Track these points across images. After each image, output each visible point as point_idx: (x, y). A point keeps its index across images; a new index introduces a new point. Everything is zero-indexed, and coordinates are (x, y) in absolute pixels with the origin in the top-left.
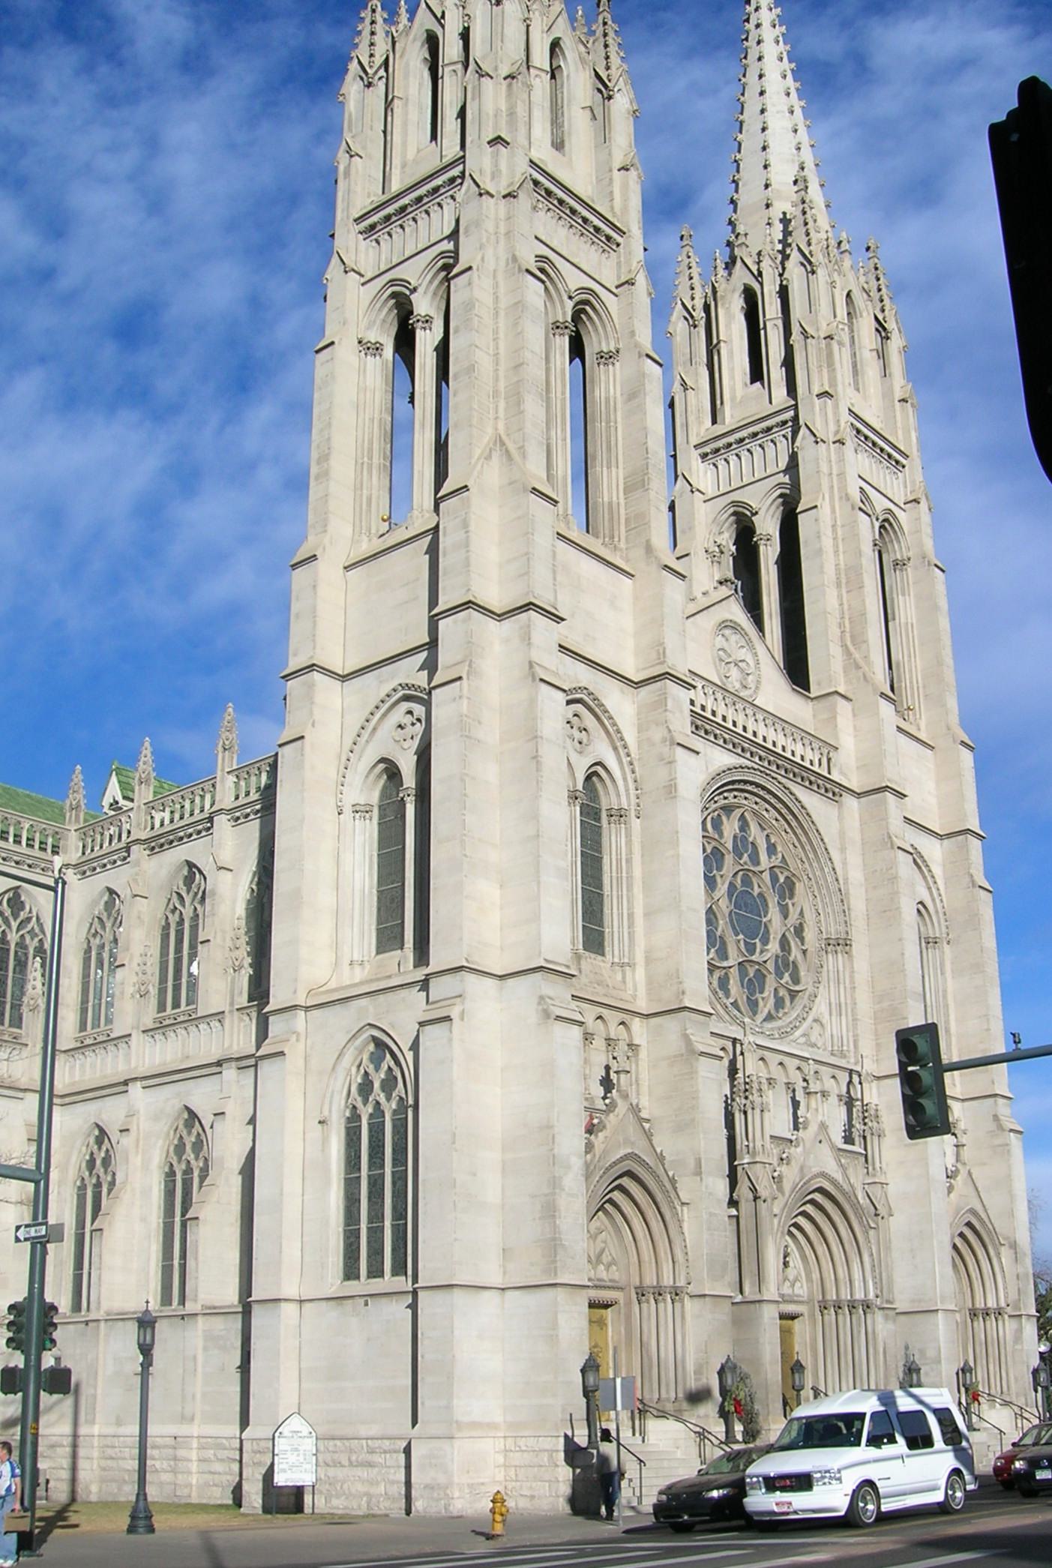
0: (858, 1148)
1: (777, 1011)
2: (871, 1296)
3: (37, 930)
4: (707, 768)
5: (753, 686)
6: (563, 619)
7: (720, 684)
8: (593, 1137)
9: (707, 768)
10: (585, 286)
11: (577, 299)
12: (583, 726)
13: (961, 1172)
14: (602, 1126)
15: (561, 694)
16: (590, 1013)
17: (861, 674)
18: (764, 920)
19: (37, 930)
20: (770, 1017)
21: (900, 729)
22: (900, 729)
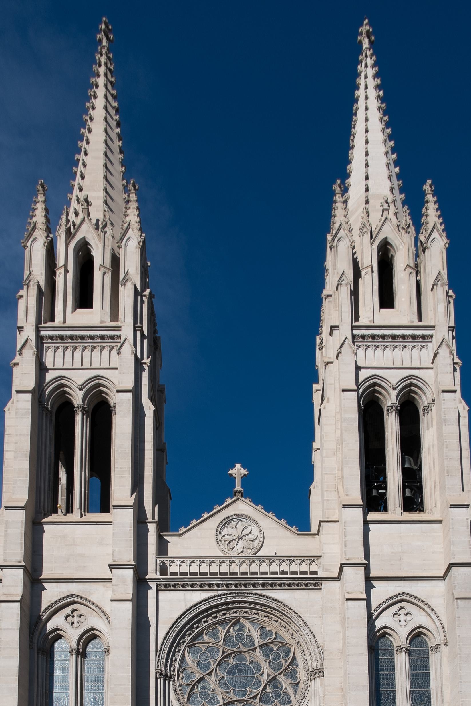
18: (248, 663)
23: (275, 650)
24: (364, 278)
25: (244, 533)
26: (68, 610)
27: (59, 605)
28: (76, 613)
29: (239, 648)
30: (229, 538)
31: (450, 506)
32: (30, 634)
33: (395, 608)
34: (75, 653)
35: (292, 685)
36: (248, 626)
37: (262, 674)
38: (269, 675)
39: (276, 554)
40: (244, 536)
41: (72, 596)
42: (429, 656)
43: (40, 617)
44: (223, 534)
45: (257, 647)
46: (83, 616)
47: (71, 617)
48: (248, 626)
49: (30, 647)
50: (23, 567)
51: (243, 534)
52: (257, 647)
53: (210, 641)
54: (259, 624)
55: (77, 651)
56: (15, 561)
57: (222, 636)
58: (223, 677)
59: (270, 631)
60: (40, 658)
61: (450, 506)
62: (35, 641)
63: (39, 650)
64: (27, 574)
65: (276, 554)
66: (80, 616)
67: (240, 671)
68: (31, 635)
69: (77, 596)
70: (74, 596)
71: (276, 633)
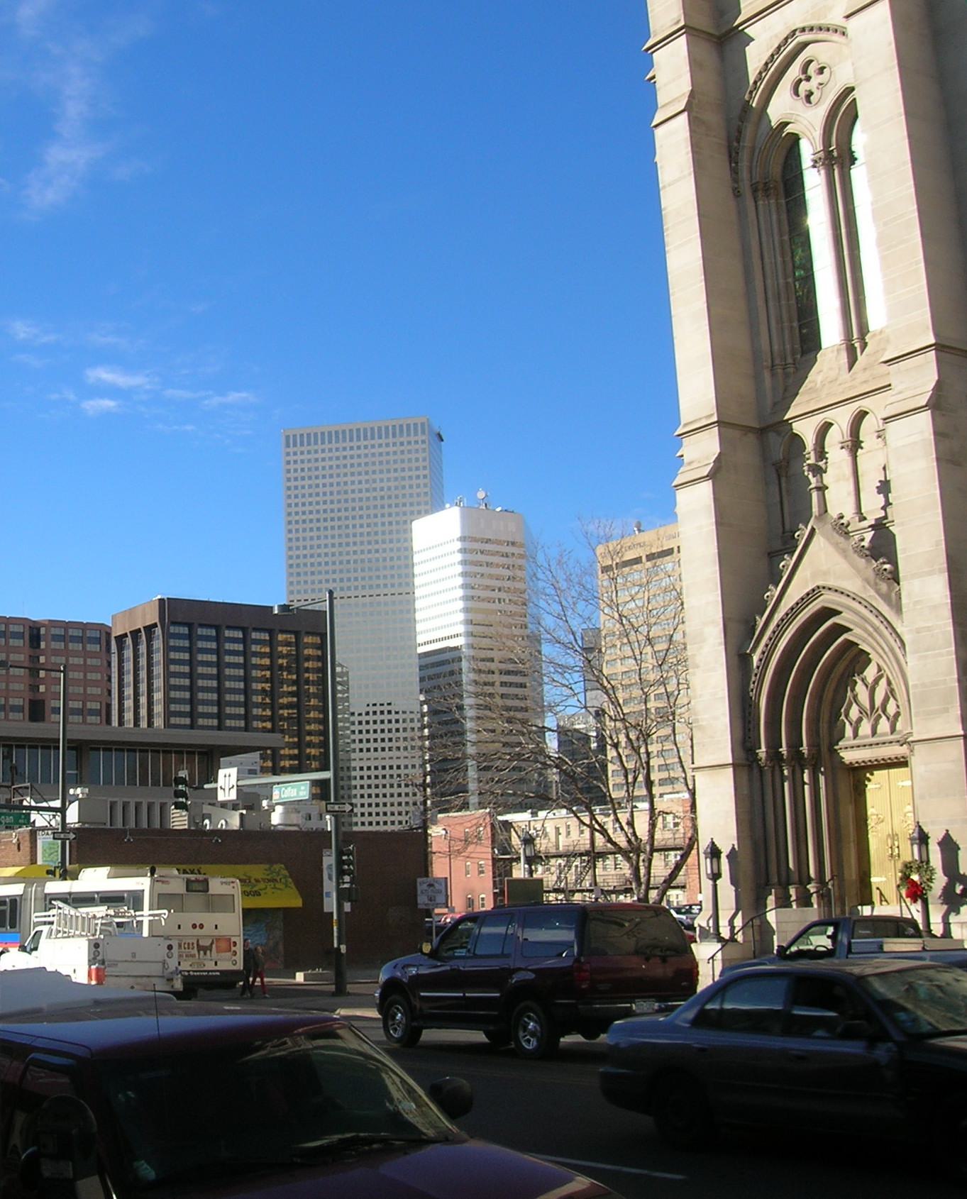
26: (794, 72)
27: (772, 69)
28: (812, 69)
31: (935, 837)
32: (730, 163)
34: (823, 165)
39: (134, 955)
41: (794, 34)
43: (747, 104)
46: (824, 68)
47: (803, 82)
49: (734, 195)
50: (683, 31)
53: (642, 755)
55: (826, 159)
56: (669, 24)
60: (761, 208)
61: (935, 837)
62: (744, 174)
63: (755, 191)
64: (698, 36)
65: (134, 955)
66: (821, 70)
68: (733, 165)
69: (803, 30)
70: (797, 33)
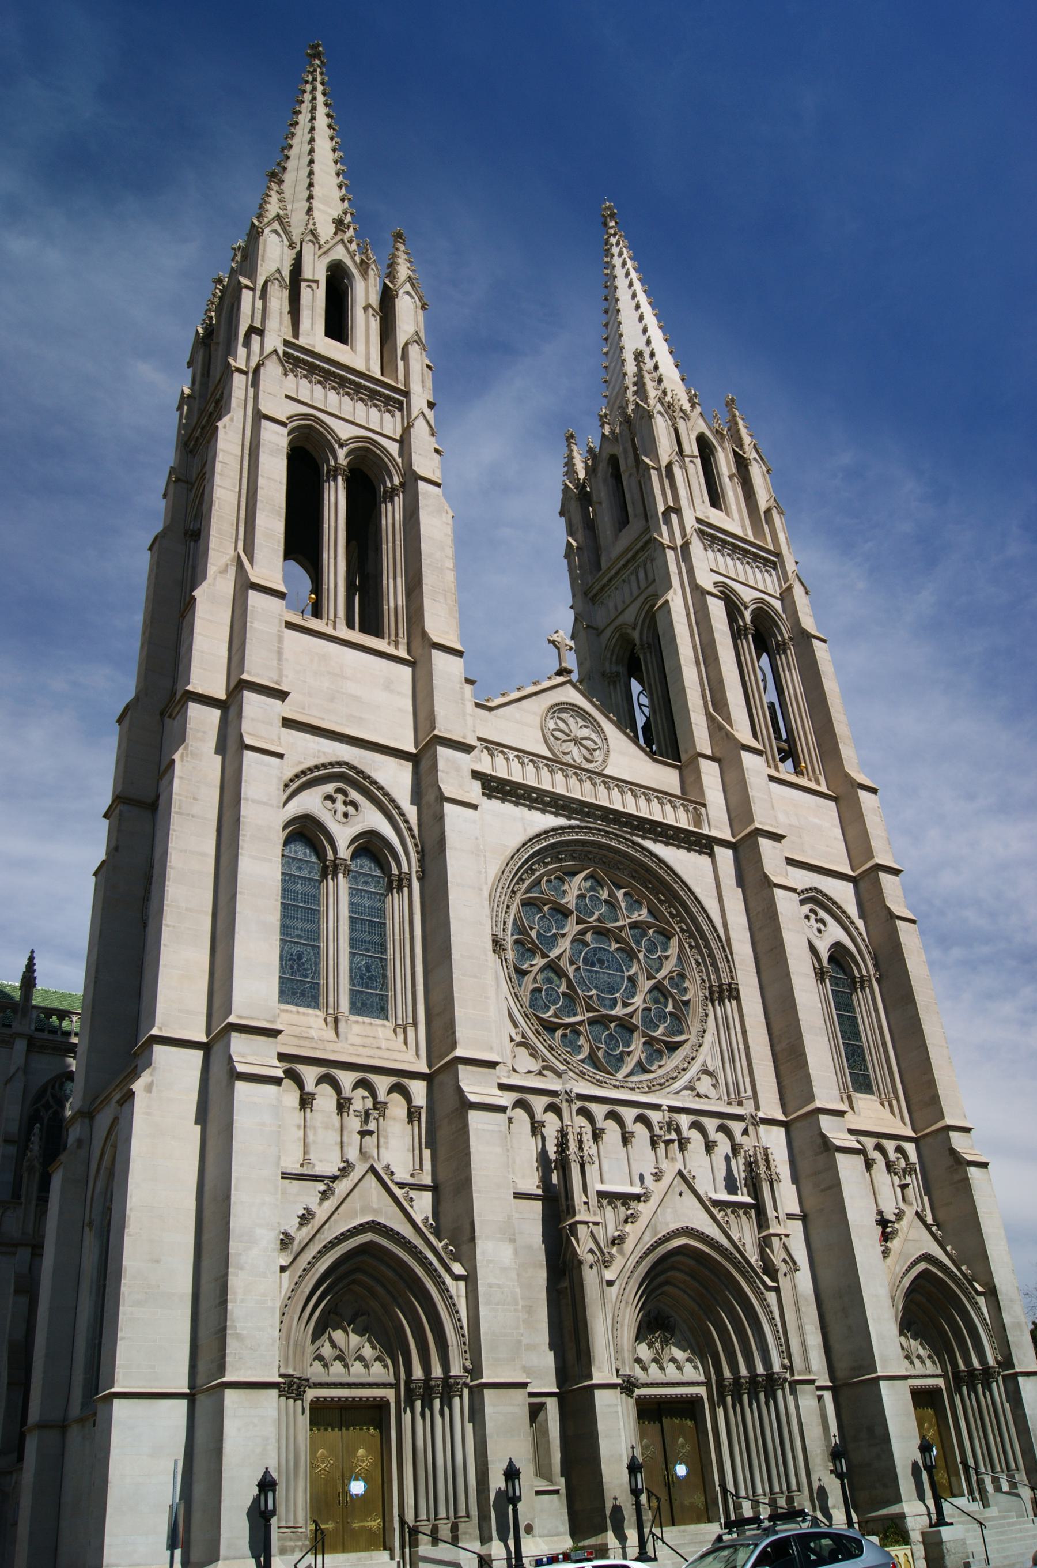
0: (743, 1197)
1: (651, 1063)
2: (777, 1368)
3: (51, 1102)
4: (525, 830)
5: (600, 759)
6: (783, 837)
7: (550, 755)
8: (889, 1244)
9: (525, 830)
10: (352, 435)
11: (290, 426)
12: (348, 799)
13: (907, 1213)
14: (895, 1233)
15: (794, 895)
16: (869, 1143)
17: (724, 733)
18: (627, 974)
19: (51, 1102)
20: (642, 1068)
21: (772, 778)
22: (772, 778)
23: (667, 1010)
24: (422, 367)
25: (584, 742)
29: (639, 951)
30: (562, 725)
33: (330, 788)
35: (639, 1063)
36: (673, 950)
37: (625, 1005)
38: (631, 1015)
40: (581, 744)
42: (385, 919)
44: (559, 715)
45: (656, 978)
48: (673, 950)
51: (582, 742)
52: (656, 978)
54: (683, 966)
57: (635, 917)
58: (586, 944)
59: (686, 990)
67: (601, 962)
71: (689, 1001)
